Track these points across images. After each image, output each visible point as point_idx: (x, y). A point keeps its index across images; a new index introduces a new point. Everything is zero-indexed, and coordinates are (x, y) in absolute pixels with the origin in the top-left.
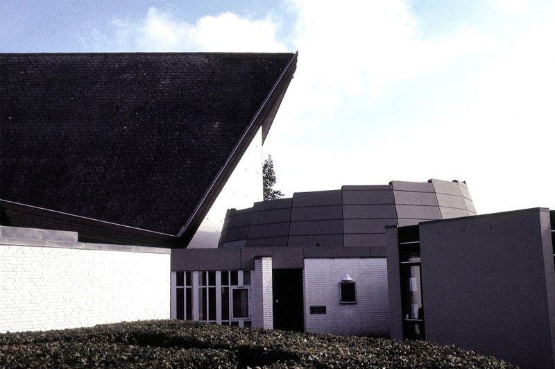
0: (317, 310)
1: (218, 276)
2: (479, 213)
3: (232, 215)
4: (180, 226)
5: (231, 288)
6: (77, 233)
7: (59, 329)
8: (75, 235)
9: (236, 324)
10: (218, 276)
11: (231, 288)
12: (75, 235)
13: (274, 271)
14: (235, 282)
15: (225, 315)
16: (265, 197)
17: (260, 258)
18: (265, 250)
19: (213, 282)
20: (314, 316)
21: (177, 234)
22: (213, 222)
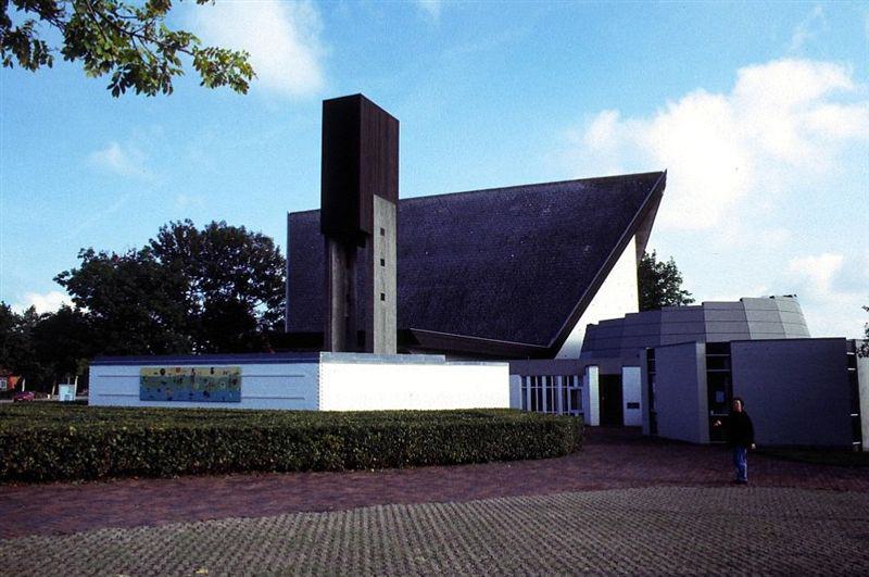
0: (631, 406)
1: (544, 379)
2: (812, 337)
3: (590, 327)
4: (550, 338)
5: (569, 388)
6: (633, 306)
7: (419, 409)
8: (443, 357)
9: (572, 414)
10: (544, 379)
11: (569, 388)
12: (346, 315)
13: (600, 376)
14: (572, 384)
15: (566, 408)
16: (87, 372)
17: (588, 366)
18: (595, 361)
19: (540, 384)
20: (630, 410)
21: (547, 344)
22: (577, 335)
